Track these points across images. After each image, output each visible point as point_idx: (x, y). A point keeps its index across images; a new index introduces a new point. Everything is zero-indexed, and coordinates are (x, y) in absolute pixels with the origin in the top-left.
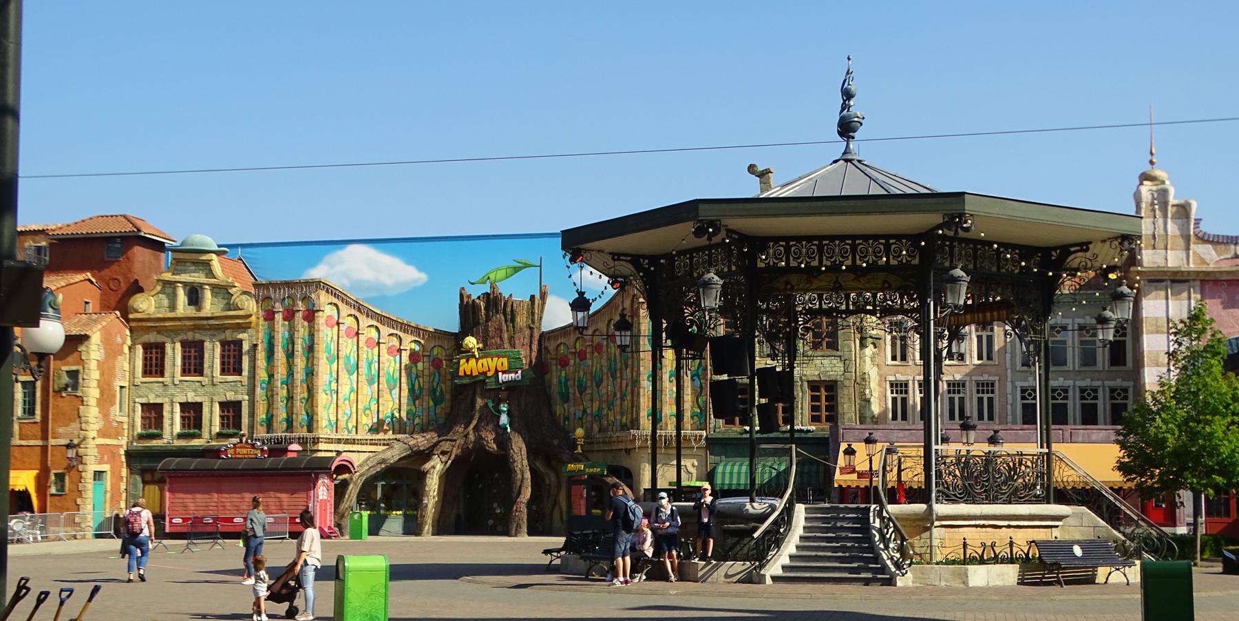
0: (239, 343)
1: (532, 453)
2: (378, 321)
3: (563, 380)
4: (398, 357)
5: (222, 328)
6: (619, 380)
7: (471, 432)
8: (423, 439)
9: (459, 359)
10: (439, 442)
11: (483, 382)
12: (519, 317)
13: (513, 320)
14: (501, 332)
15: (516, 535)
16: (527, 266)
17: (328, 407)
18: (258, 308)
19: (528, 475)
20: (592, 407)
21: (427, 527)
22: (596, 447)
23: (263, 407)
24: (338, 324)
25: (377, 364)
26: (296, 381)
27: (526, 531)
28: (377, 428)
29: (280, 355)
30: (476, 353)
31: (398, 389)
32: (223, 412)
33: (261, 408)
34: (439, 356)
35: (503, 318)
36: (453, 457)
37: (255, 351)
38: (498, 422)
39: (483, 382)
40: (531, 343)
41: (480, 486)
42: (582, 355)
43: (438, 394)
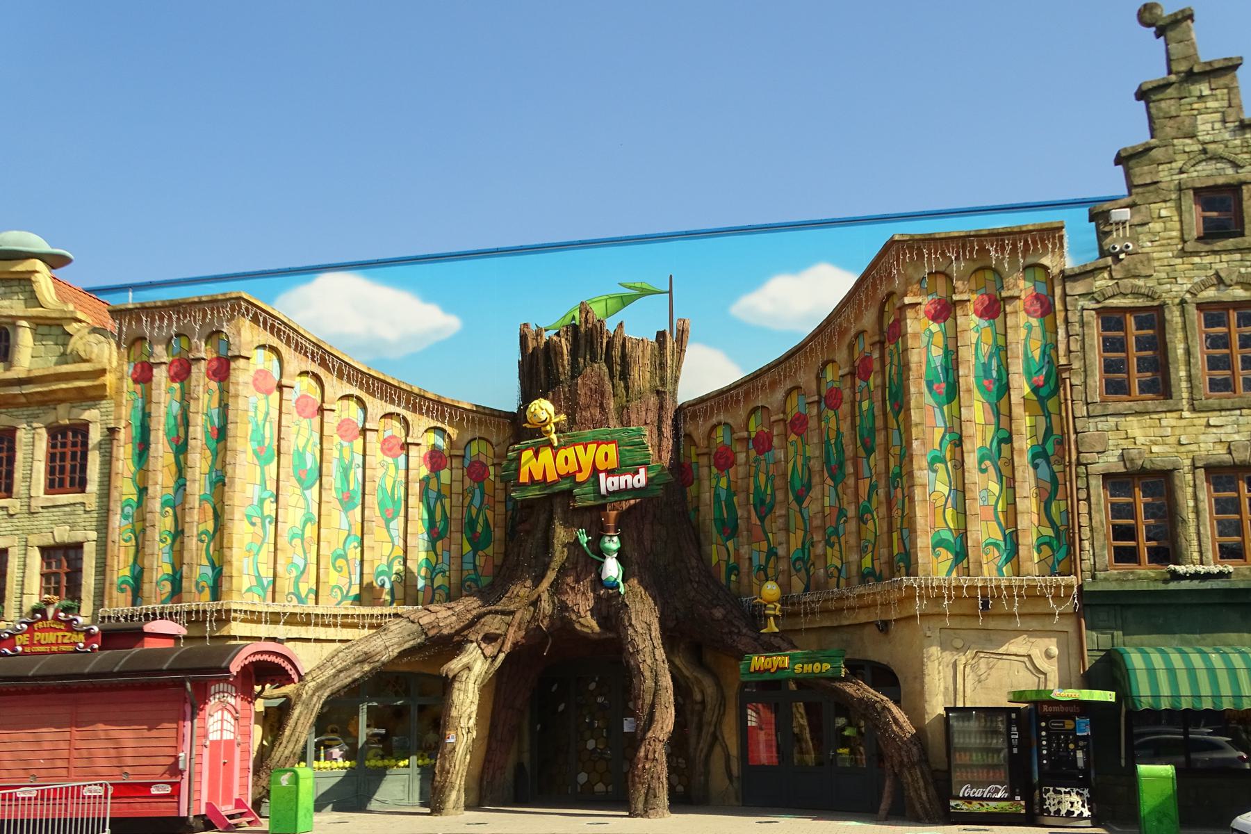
0: (82, 430)
1: (671, 638)
2: (361, 387)
3: (723, 496)
4: (402, 458)
5: (47, 401)
6: (851, 481)
7: (545, 596)
8: (450, 612)
9: (520, 452)
10: (480, 616)
11: (568, 494)
12: (636, 369)
13: (625, 375)
14: (602, 394)
15: (645, 814)
16: (644, 293)
17: (255, 548)
18: (120, 358)
19: (667, 681)
20: (788, 542)
21: (454, 795)
22: (803, 623)
23: (127, 553)
24: (280, 387)
25: (360, 471)
26: (190, 498)
27: (667, 803)
28: (367, 594)
29: (161, 449)
30: (554, 436)
31: (401, 519)
32: (49, 565)
33: (122, 557)
34: (482, 458)
35: (605, 369)
36: (508, 647)
37: (111, 441)
38: (599, 575)
39: (568, 494)
40: (660, 420)
41: (561, 707)
42: (762, 444)
43: (479, 529)
